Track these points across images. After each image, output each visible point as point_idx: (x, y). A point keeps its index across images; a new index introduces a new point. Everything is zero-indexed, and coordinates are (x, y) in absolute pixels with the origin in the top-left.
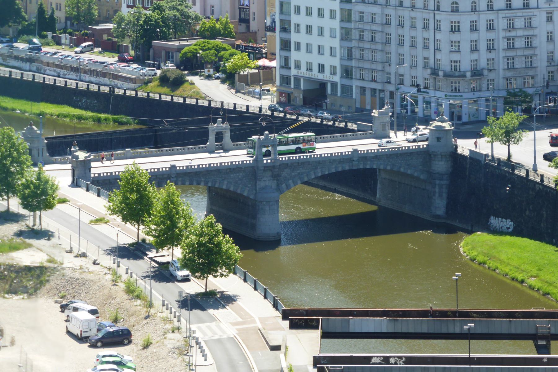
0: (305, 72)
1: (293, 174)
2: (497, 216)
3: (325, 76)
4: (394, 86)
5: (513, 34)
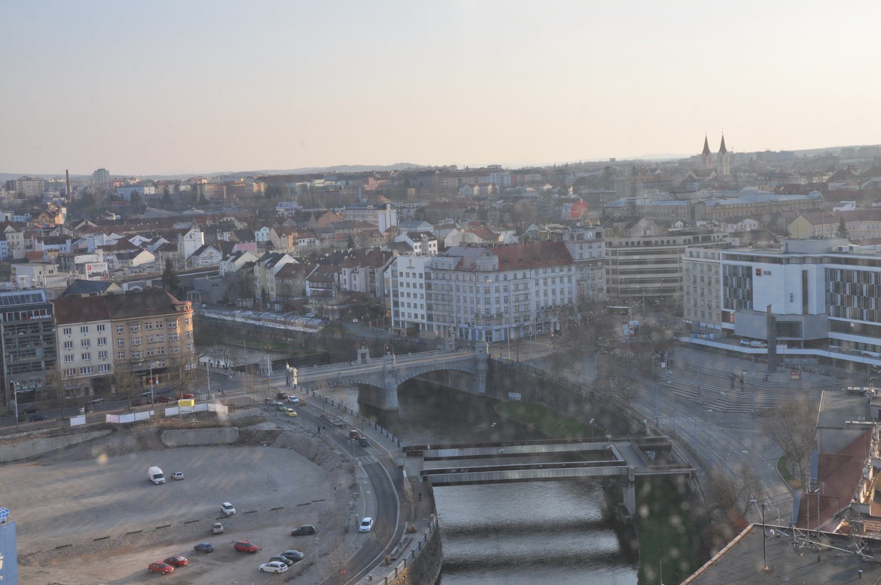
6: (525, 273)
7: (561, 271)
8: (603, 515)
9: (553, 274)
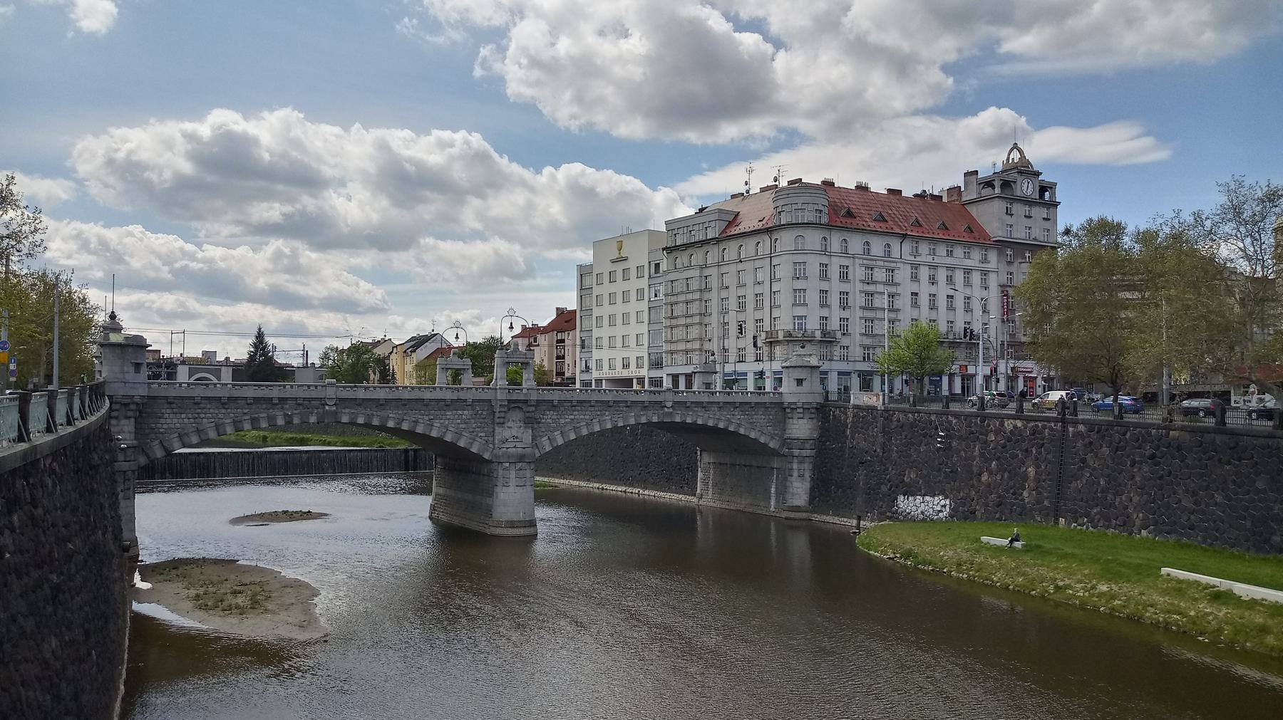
2: (910, 492)
5: (871, 288)
6: (888, 245)
7: (967, 255)
8: (490, 494)
9: (949, 261)
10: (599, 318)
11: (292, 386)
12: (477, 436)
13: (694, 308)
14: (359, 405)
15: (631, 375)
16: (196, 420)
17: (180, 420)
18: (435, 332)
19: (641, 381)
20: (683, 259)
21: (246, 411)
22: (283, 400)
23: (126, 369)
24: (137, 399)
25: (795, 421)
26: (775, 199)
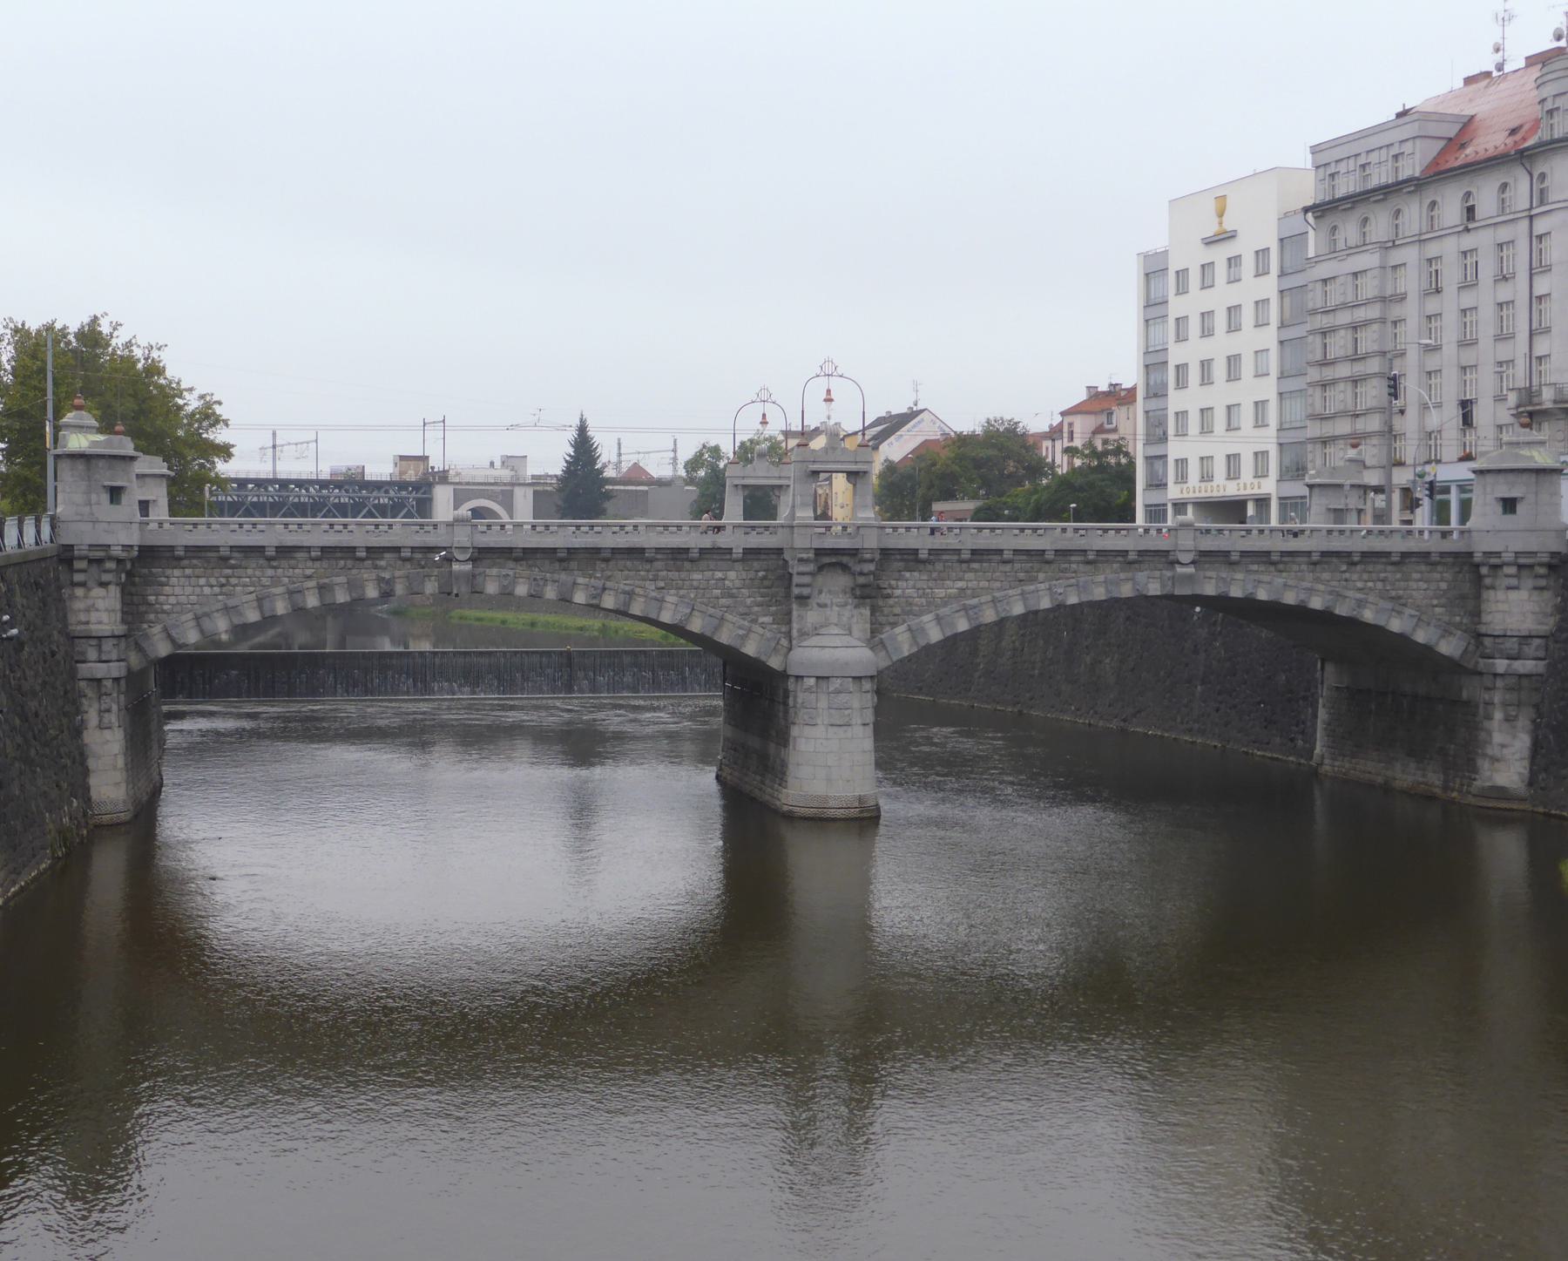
0: (1197, 485)
1: (940, 593)
3: (1242, 485)
4: (1412, 469)
10: (1181, 369)
11: (1159, 530)
12: (754, 621)
13: (1369, 340)
14: (516, 560)
15: (1242, 492)
16: (224, 589)
17: (198, 590)
18: (920, 407)
19: (1262, 502)
20: (1349, 230)
21: (309, 572)
22: (374, 552)
23: (94, 497)
24: (117, 552)
25: (1501, 595)
26: (1539, 82)
